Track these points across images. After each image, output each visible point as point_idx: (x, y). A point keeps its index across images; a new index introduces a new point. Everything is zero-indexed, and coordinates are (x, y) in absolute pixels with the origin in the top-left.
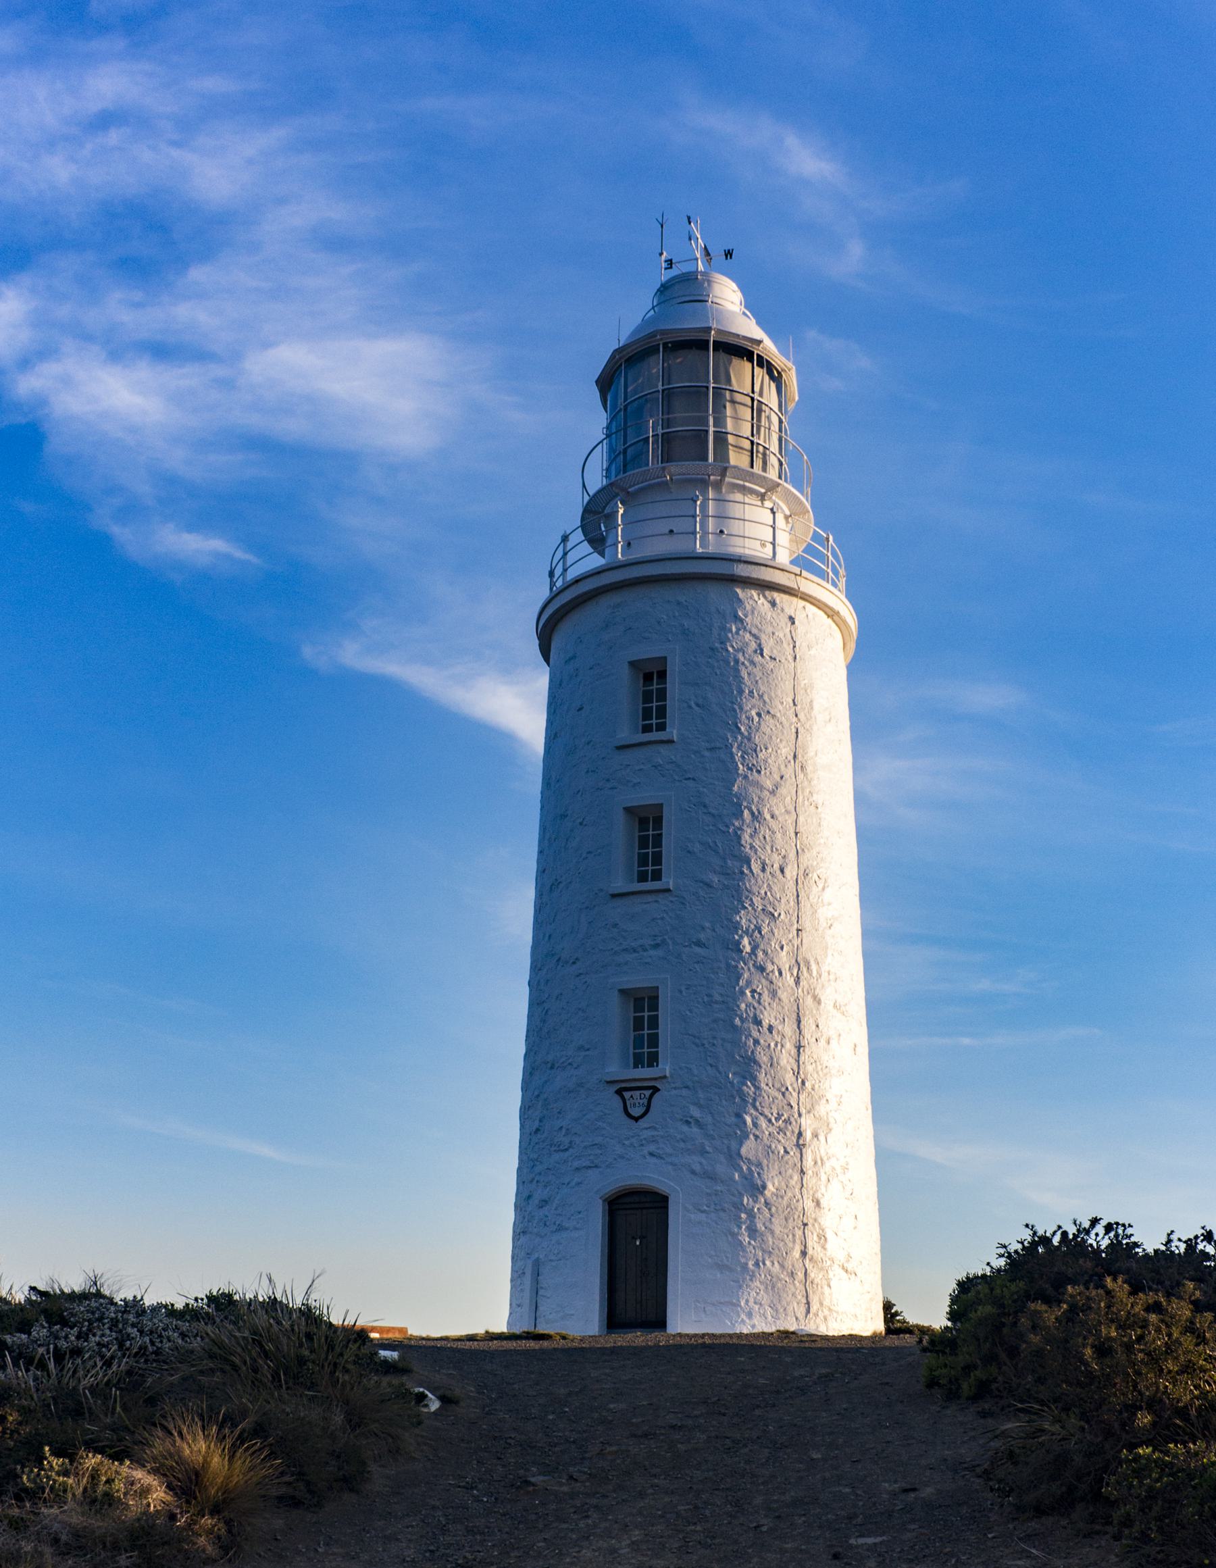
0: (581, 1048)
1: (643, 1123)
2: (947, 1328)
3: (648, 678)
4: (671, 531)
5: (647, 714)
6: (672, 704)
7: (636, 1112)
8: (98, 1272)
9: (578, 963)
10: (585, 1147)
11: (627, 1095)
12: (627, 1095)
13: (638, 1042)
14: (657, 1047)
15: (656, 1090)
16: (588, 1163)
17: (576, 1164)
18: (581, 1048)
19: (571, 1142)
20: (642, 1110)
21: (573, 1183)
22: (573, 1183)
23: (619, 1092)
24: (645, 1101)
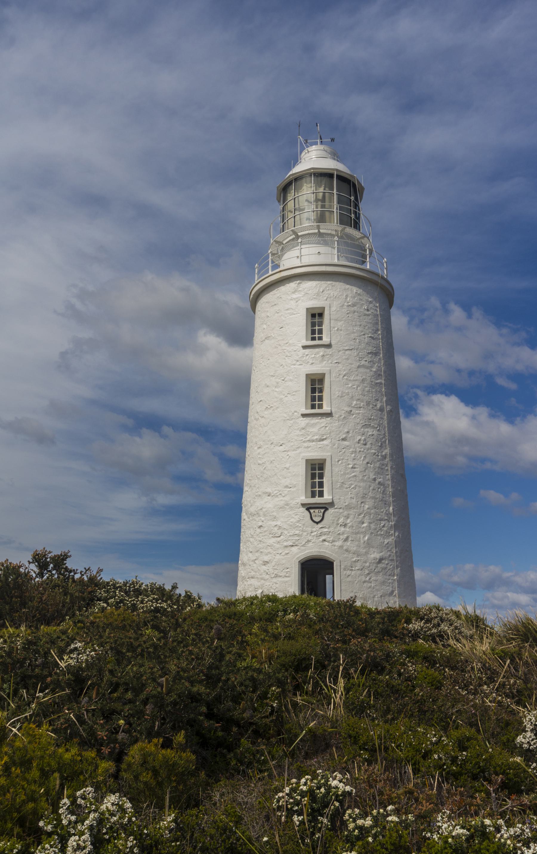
0: (287, 487)
1: (320, 525)
2: (295, 596)
3: (313, 316)
4: (319, 253)
5: (313, 332)
6: (325, 327)
7: (317, 519)
8: (40, 549)
9: (284, 446)
10: (290, 536)
11: (322, 510)
12: (312, 511)
13: (313, 485)
14: (323, 488)
15: (326, 509)
16: (291, 544)
17: (285, 544)
18: (287, 487)
19: (282, 533)
20: (320, 519)
21: (283, 554)
22: (283, 554)
23: (308, 509)
24: (321, 514)
